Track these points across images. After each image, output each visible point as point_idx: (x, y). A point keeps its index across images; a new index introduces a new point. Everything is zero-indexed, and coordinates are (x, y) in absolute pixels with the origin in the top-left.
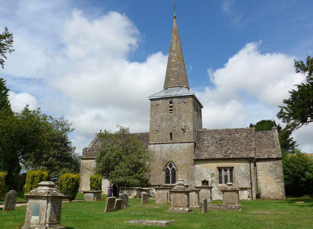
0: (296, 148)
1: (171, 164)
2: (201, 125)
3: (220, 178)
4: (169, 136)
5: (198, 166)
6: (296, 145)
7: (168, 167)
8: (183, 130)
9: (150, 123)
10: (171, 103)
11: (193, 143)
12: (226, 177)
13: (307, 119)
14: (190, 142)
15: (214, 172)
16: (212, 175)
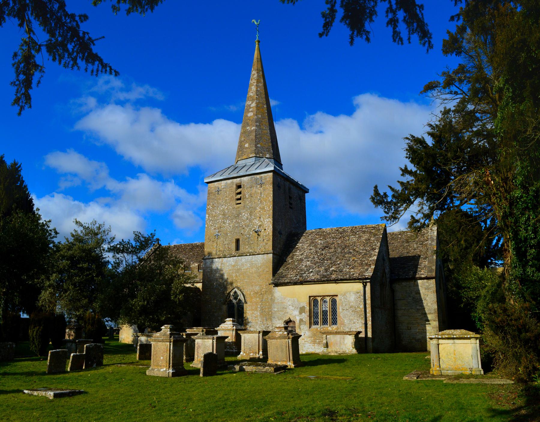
1: (235, 292)
4: (233, 246)
11: (271, 174)
12: (325, 313)
16: (302, 310)
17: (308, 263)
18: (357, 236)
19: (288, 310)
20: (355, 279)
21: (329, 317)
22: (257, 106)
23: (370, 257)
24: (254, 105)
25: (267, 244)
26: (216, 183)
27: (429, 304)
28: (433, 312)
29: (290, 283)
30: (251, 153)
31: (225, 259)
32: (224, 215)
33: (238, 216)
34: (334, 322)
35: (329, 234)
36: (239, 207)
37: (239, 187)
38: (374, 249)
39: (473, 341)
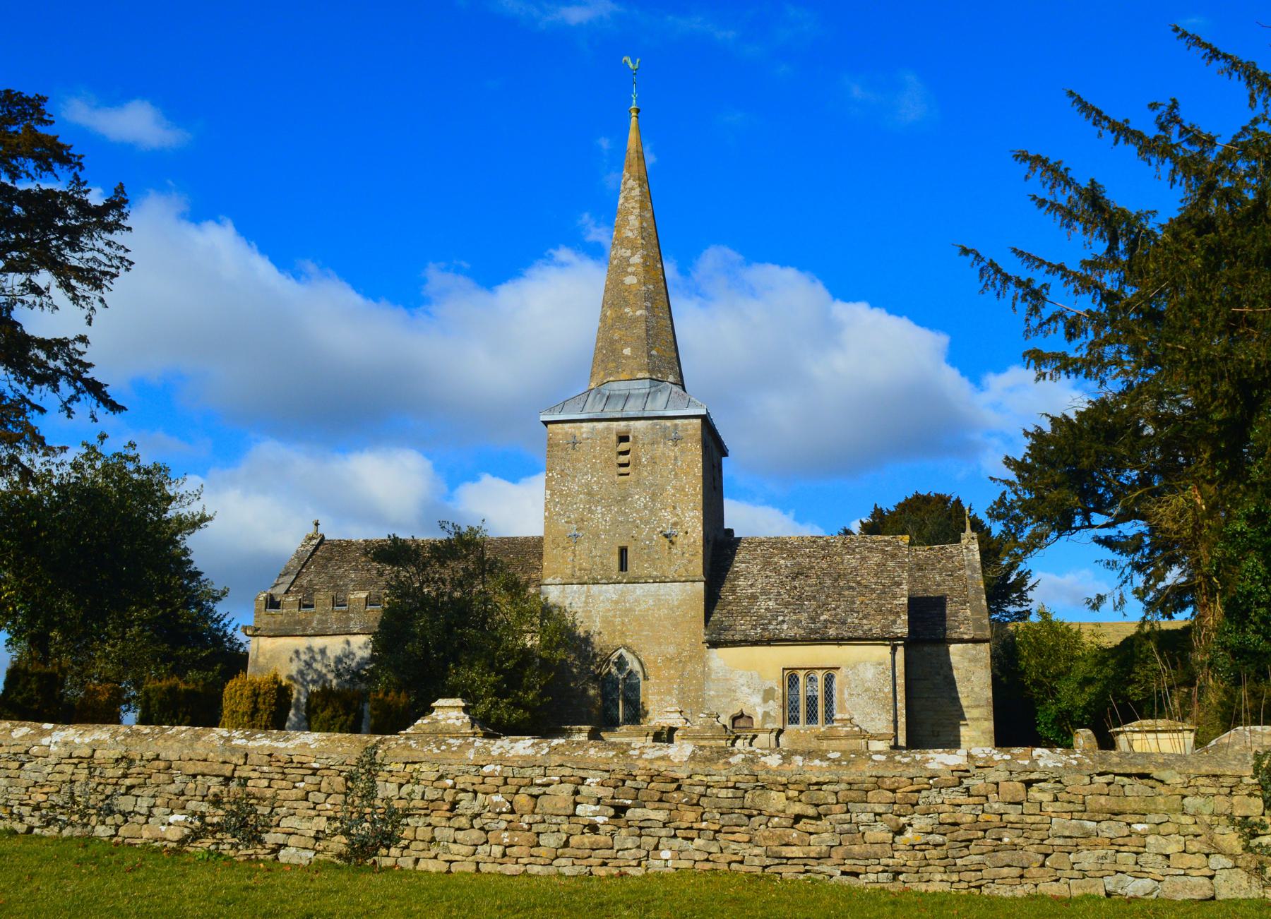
0: (1030, 595)
1: (621, 656)
4: (614, 561)
6: (1030, 584)
9: (547, 509)
11: (699, 421)
12: (812, 701)
13: (1071, 520)
16: (768, 695)
17: (770, 603)
19: (739, 695)
20: (877, 639)
22: (645, 264)
23: (895, 597)
24: (637, 259)
25: (690, 561)
26: (567, 426)
27: (977, 689)
28: (982, 703)
29: (746, 641)
30: (640, 370)
31: (595, 588)
32: (589, 494)
35: (799, 548)
36: (625, 482)
37: (623, 438)
38: (899, 584)
39: (1187, 734)
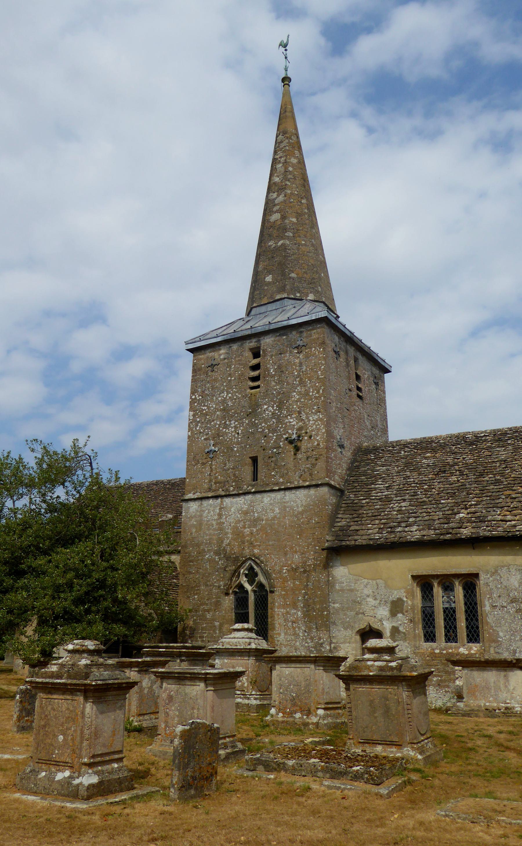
1: (251, 569)
2: (385, 430)
3: (428, 618)
4: (247, 471)
5: (342, 572)
7: (244, 581)
8: (291, 442)
10: (256, 354)
12: (450, 614)
14: (317, 486)
15: (401, 594)
16: (396, 607)
17: (403, 504)
18: (510, 448)
21: (462, 623)
33: (254, 411)
34: (474, 636)
